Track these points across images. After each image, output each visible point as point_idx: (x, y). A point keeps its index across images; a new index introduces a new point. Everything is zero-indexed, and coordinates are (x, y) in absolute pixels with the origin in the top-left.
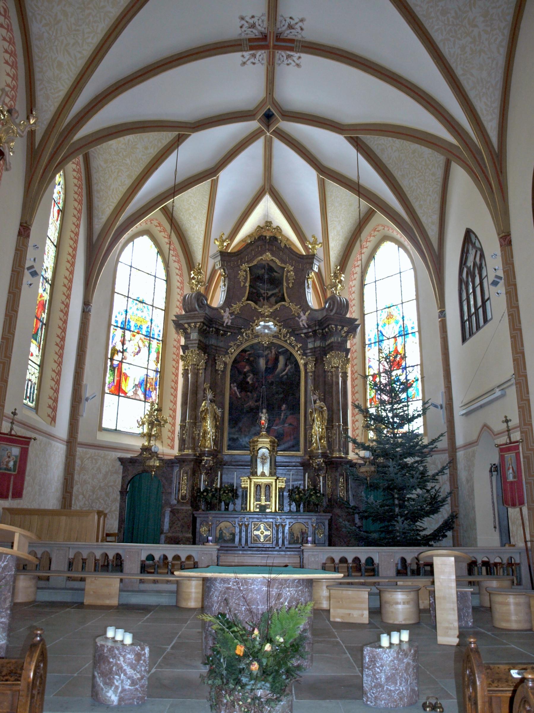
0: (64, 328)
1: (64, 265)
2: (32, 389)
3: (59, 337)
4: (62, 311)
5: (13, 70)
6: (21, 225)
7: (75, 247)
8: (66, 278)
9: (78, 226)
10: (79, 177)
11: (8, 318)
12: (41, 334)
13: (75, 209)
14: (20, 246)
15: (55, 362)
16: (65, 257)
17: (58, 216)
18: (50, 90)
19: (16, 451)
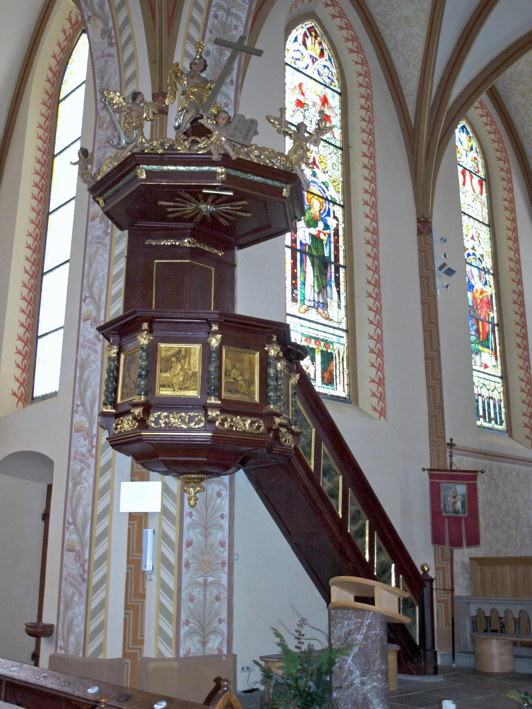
0: (523, 323)
1: (505, 244)
2: (497, 408)
3: (519, 336)
4: (515, 302)
5: (359, 55)
6: (419, 221)
7: (513, 218)
8: (511, 260)
9: (511, 190)
10: (495, 130)
11: (428, 334)
12: (495, 338)
13: (502, 170)
14: (423, 246)
15: (521, 368)
16: (503, 234)
17: (482, 188)
18: (407, 53)
19: (461, 489)
